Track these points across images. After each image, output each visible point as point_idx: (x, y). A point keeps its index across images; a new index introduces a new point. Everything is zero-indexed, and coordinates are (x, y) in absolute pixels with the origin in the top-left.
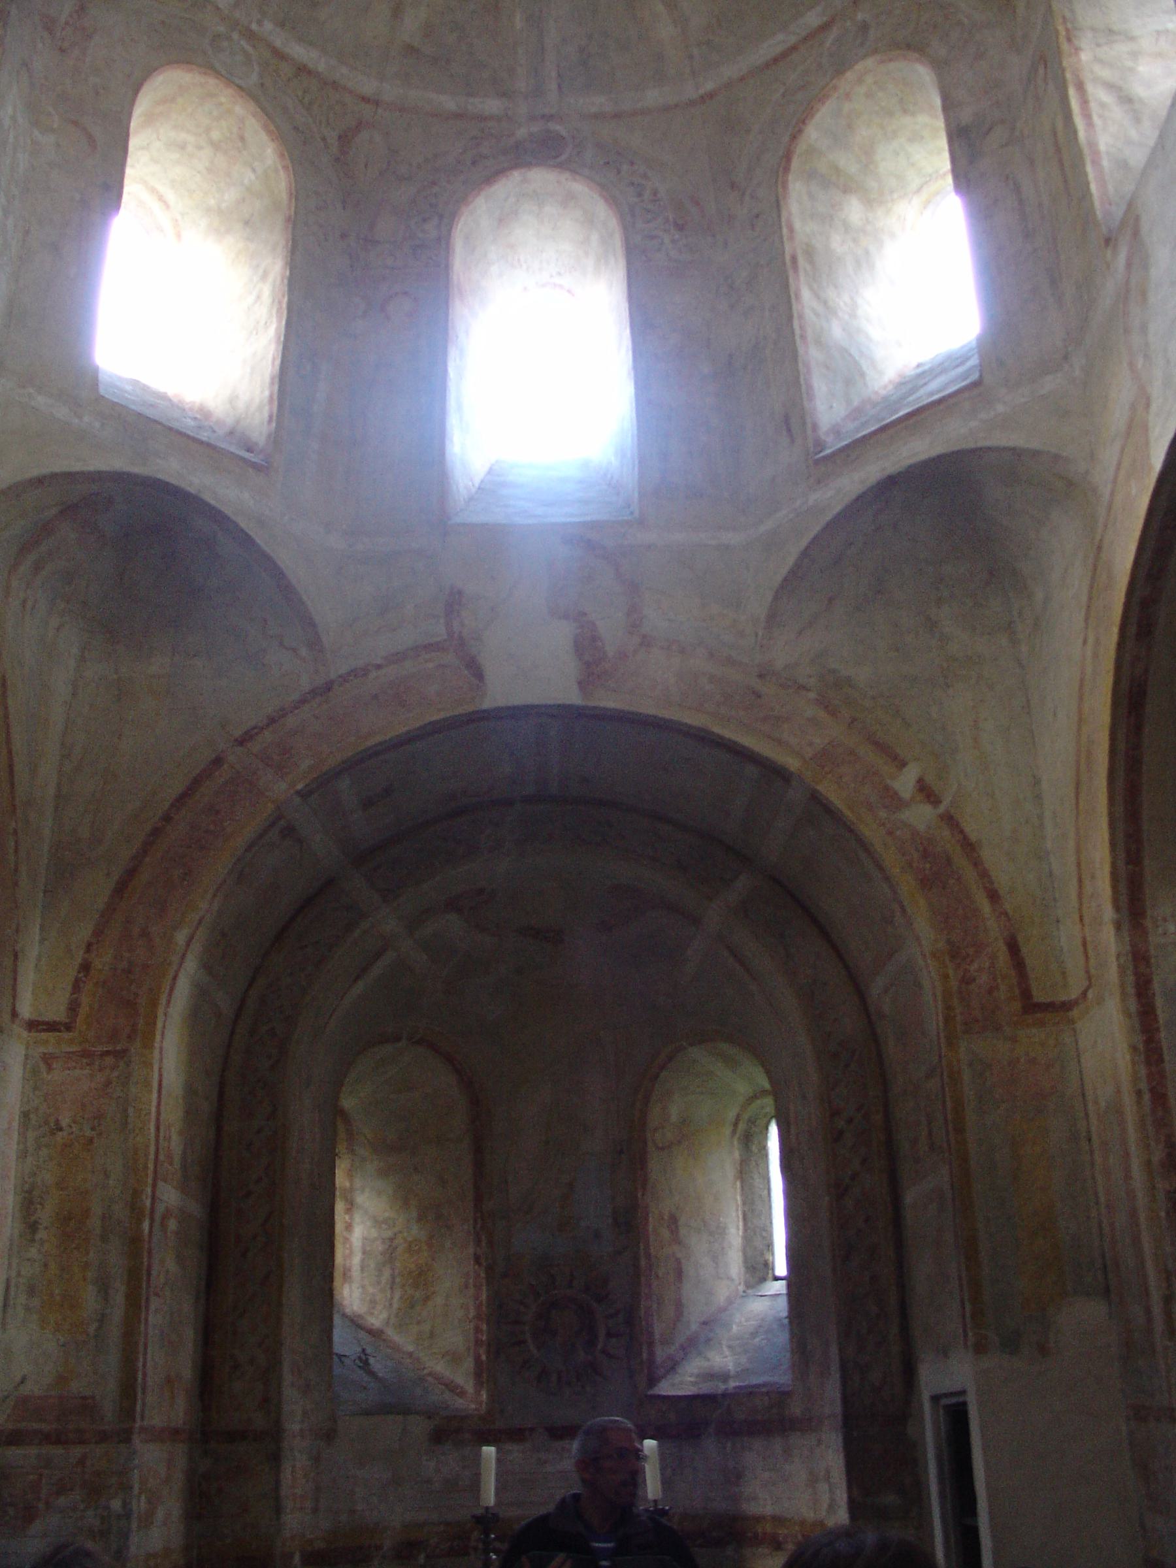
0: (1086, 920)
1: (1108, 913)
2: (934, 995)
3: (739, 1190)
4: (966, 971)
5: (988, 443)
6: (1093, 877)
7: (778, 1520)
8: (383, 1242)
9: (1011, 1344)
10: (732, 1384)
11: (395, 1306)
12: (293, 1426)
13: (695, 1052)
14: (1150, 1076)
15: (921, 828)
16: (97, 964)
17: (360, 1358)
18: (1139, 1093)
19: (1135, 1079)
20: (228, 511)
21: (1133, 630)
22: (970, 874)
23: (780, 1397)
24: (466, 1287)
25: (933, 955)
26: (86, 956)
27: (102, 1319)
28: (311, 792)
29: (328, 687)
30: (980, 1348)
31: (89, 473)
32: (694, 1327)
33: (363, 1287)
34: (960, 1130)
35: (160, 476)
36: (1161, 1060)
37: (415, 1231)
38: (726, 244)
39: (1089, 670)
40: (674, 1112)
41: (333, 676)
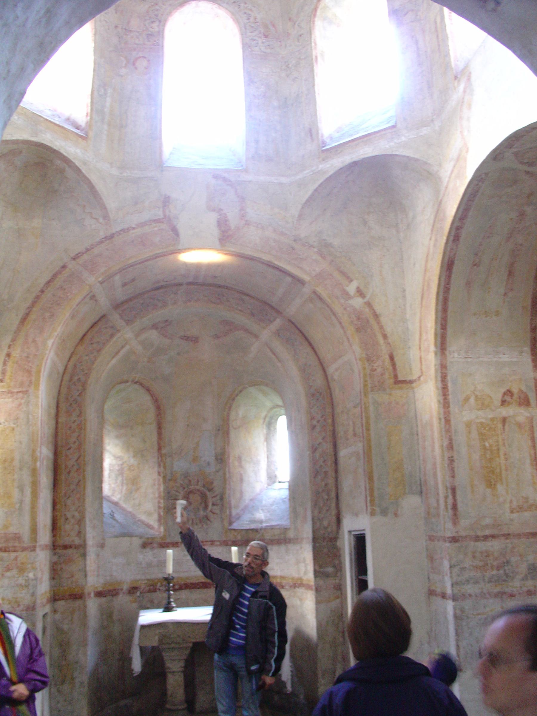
0: (422, 349)
1: (432, 348)
2: (359, 375)
3: (265, 446)
4: (373, 366)
5: (398, 153)
6: (427, 333)
7: (282, 577)
8: (118, 465)
9: (384, 512)
10: (264, 525)
11: (124, 492)
12: (90, 542)
13: (252, 390)
14: (445, 413)
15: (357, 307)
16: (14, 354)
17: (111, 514)
18: (440, 419)
19: (439, 413)
20: (71, 158)
21: (452, 238)
22: (376, 327)
23: (286, 530)
24: (155, 485)
25: (360, 359)
26: (8, 350)
27: (21, 502)
28: (104, 282)
29: (112, 236)
30: (373, 514)
31: (14, 140)
32: (247, 502)
33: (110, 484)
34: (368, 430)
35: (43, 142)
36: (449, 407)
37: (132, 461)
38: (286, 46)
39: (431, 251)
40: (241, 413)
41: (114, 231)
